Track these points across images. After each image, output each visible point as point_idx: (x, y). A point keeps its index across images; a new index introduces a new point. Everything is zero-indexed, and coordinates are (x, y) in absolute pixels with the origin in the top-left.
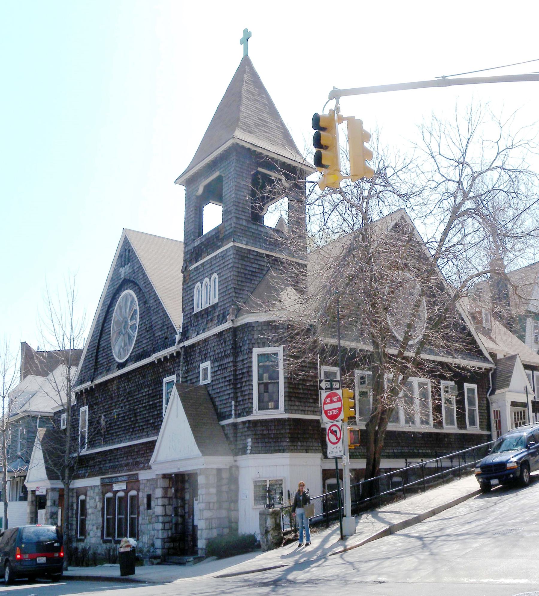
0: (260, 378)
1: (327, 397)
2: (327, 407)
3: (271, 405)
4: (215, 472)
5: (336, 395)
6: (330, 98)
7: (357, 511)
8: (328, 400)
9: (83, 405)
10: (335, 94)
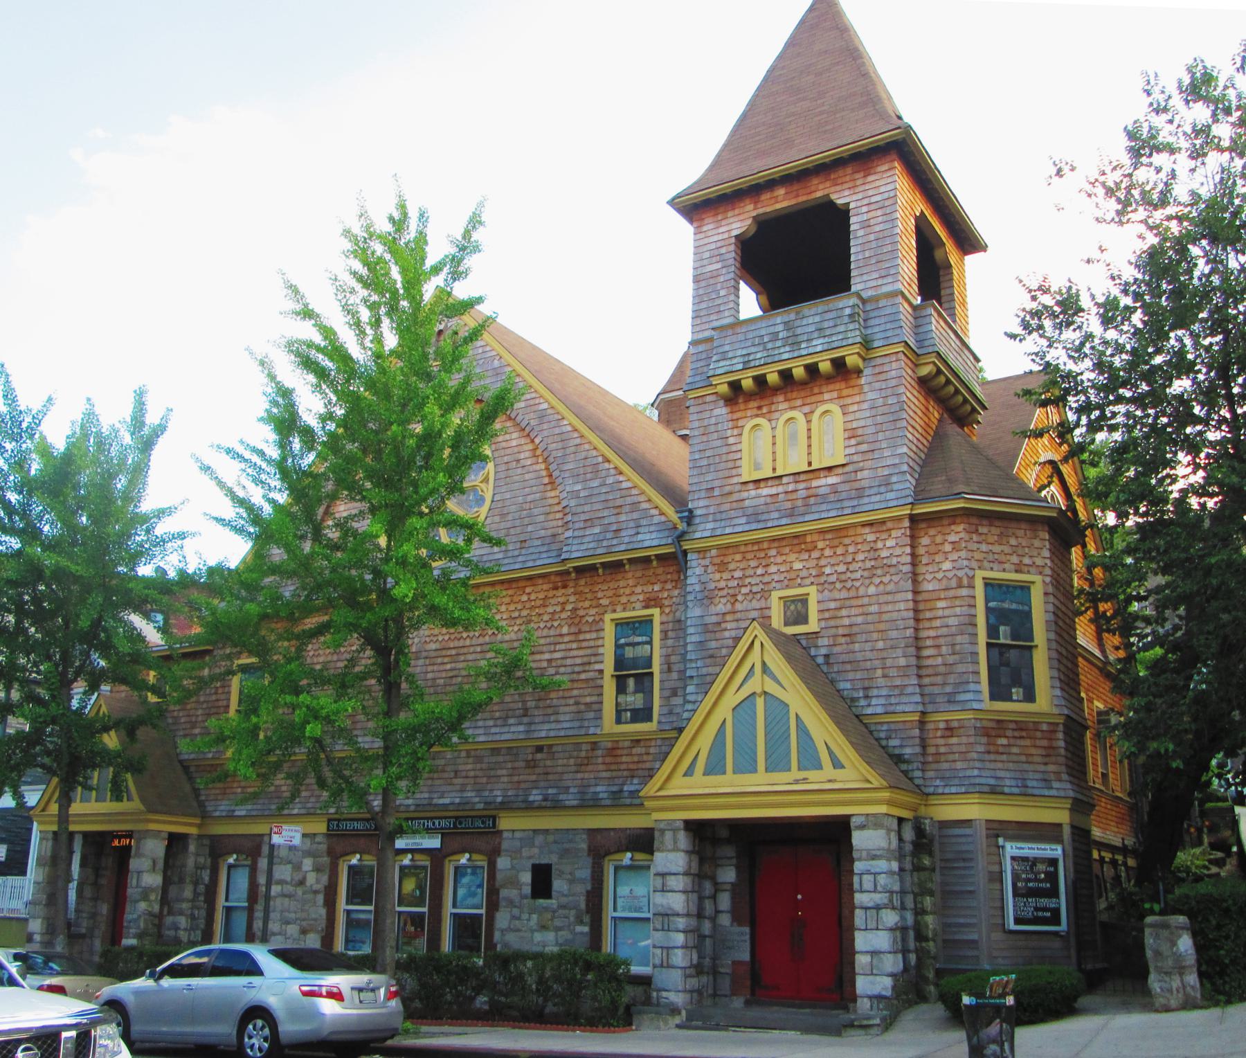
0: (992, 631)
3: (1017, 692)
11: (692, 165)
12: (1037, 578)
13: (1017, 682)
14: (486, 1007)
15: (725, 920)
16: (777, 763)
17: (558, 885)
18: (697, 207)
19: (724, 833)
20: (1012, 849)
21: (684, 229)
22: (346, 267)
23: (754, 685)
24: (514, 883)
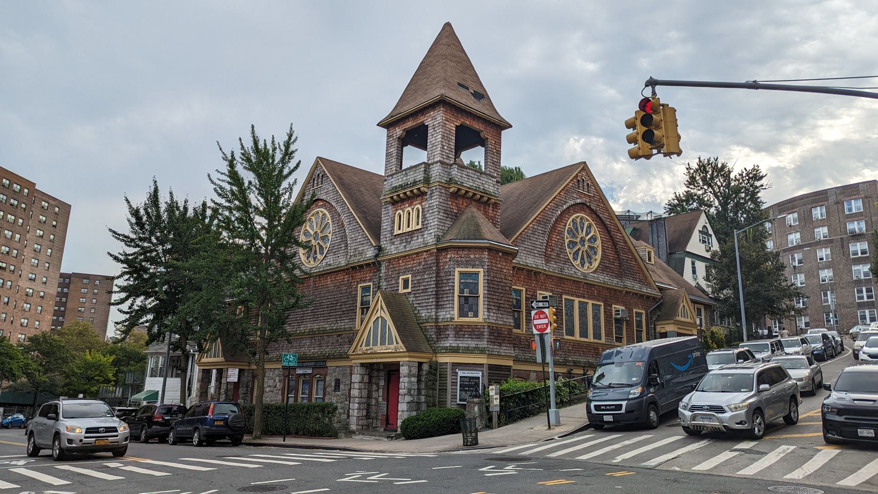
0: (461, 291)
1: (536, 314)
2: (536, 322)
3: (470, 314)
4: (417, 365)
5: (544, 313)
6: (647, 86)
7: (561, 404)
8: (537, 317)
9: (171, 244)
10: (652, 83)
11: (386, 107)
12: (481, 270)
13: (471, 310)
14: (65, 404)
15: (380, 399)
16: (383, 343)
17: (342, 387)
18: (388, 124)
19: (382, 367)
20: (461, 373)
21: (385, 131)
22: (199, 204)
23: (378, 315)
24: (330, 385)
